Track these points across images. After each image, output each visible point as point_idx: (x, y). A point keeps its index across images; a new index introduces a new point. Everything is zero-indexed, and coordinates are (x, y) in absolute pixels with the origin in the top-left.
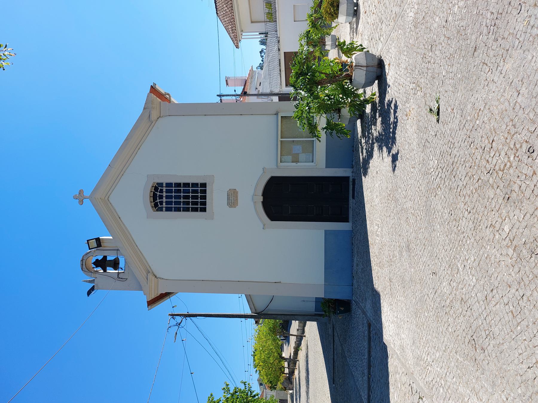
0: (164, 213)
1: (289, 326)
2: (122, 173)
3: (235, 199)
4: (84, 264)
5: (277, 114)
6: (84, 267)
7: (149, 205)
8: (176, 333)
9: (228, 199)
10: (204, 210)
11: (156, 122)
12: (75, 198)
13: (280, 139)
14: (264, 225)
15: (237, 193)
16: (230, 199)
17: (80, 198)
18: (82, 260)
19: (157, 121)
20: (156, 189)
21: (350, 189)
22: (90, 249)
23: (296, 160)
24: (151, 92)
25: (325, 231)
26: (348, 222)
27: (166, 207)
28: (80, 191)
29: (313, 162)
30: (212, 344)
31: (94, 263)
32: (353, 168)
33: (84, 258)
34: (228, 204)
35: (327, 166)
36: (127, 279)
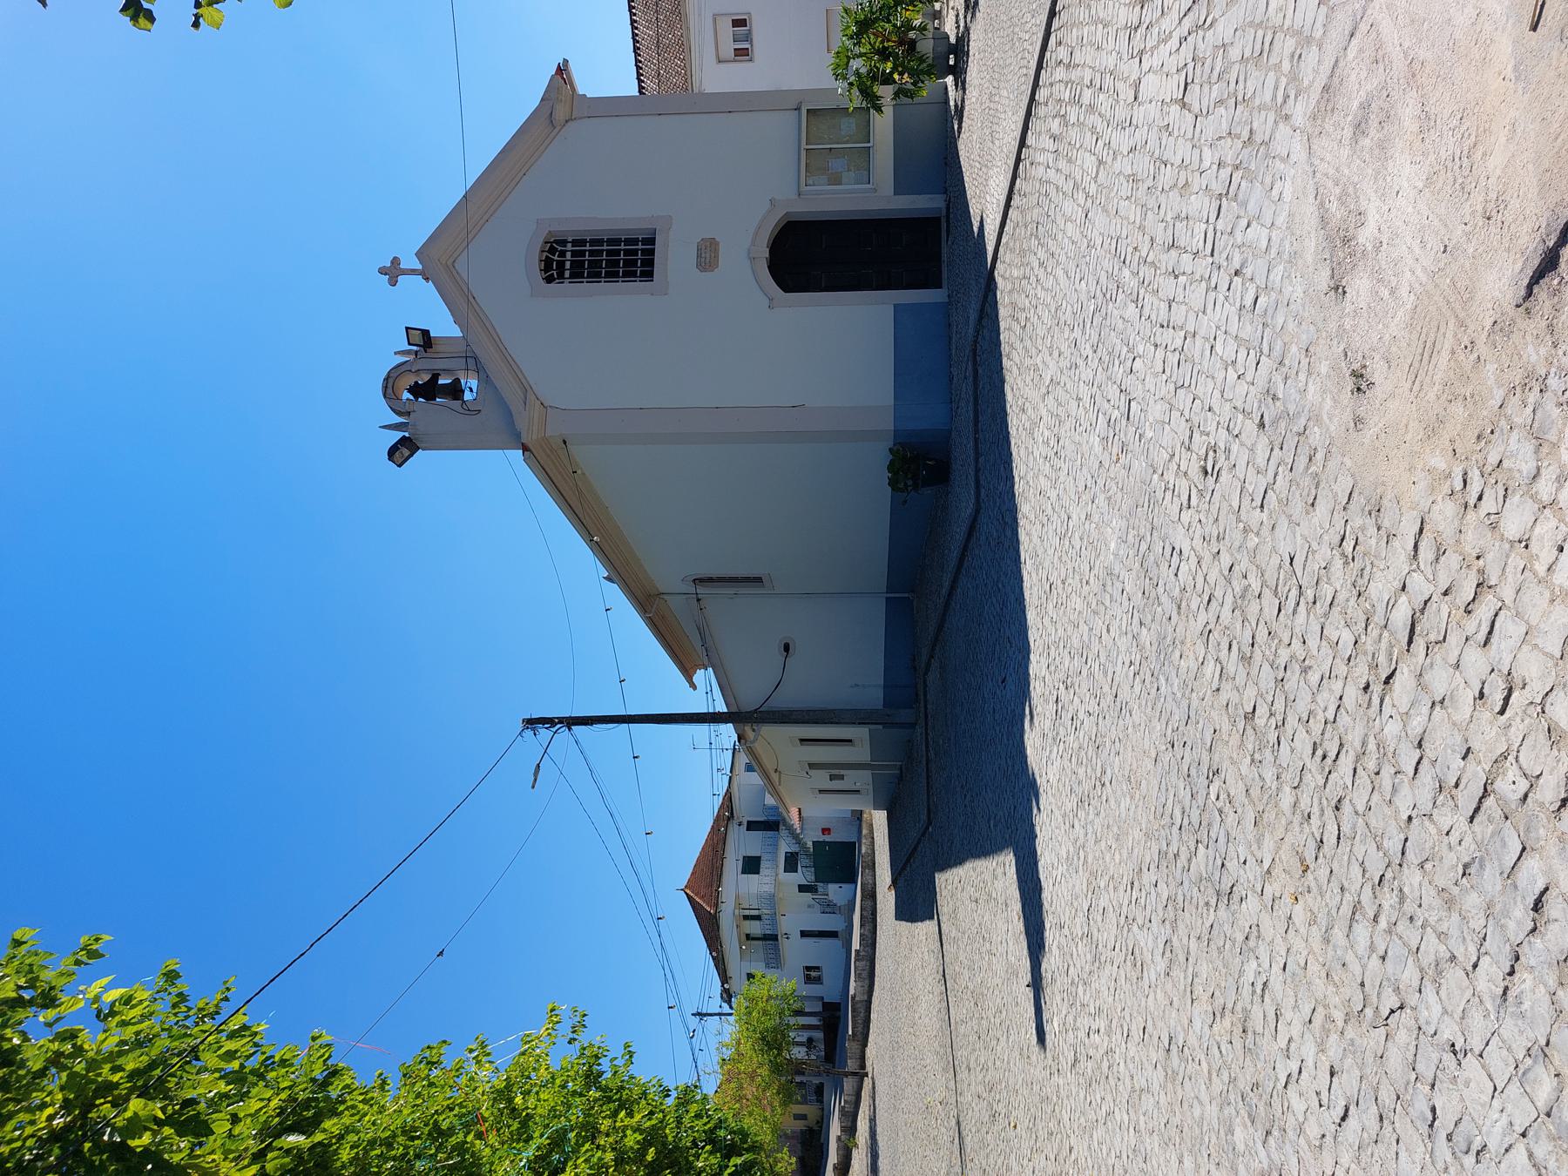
0: (567, 287)
1: (824, 1150)
2: (486, 218)
3: (713, 255)
4: (390, 385)
5: (798, 109)
6: (390, 390)
7: (538, 276)
8: (538, 765)
9: (699, 256)
10: (648, 275)
11: (562, 128)
12: (383, 271)
13: (804, 146)
14: (771, 300)
15: (717, 244)
16: (703, 255)
17: (393, 272)
18: (386, 379)
19: (565, 128)
20: (552, 250)
21: (943, 240)
22: (409, 344)
23: (836, 180)
24: (556, 73)
25: (895, 306)
26: (941, 287)
27: (572, 251)
28: (395, 258)
29: (869, 183)
30: (623, 830)
31: (410, 390)
32: (945, 193)
33: (392, 375)
34: (699, 265)
35: (898, 190)
36: (480, 411)
